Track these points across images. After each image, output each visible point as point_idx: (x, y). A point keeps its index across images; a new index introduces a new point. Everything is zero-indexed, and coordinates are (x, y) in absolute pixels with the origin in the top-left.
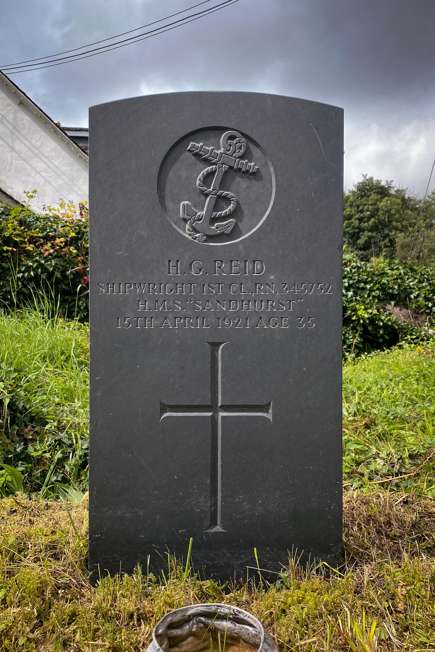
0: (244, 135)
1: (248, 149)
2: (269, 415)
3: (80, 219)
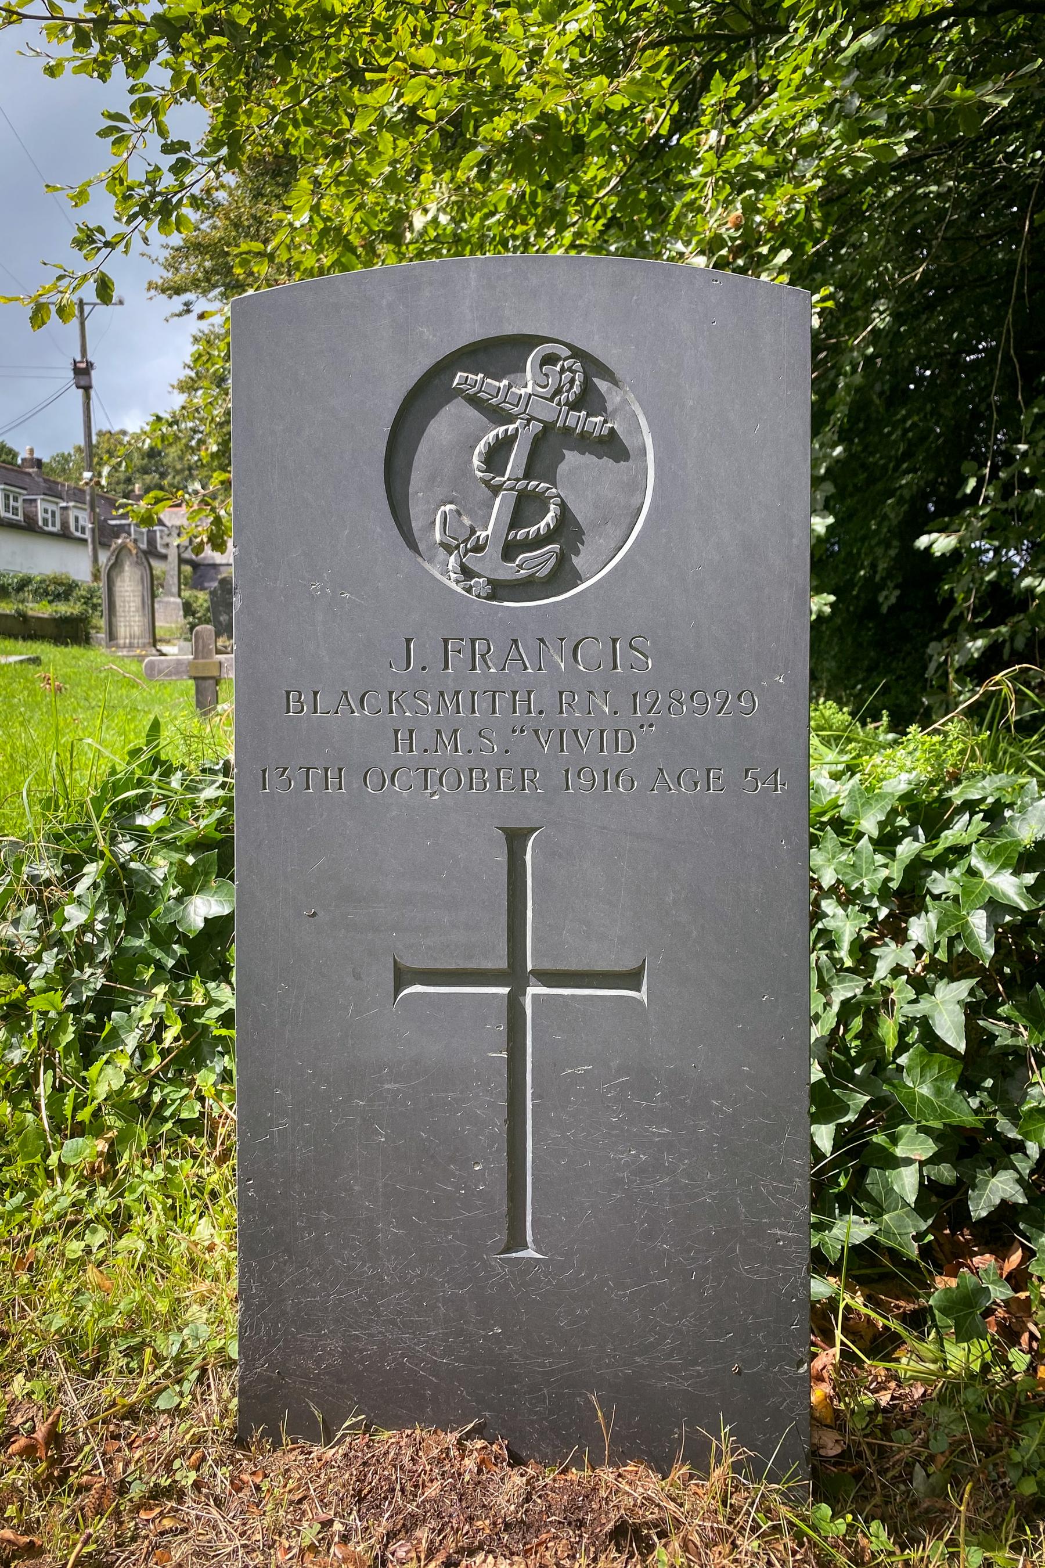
0: (577, 353)
1: (588, 386)
2: (643, 995)
3: (485, 43)
